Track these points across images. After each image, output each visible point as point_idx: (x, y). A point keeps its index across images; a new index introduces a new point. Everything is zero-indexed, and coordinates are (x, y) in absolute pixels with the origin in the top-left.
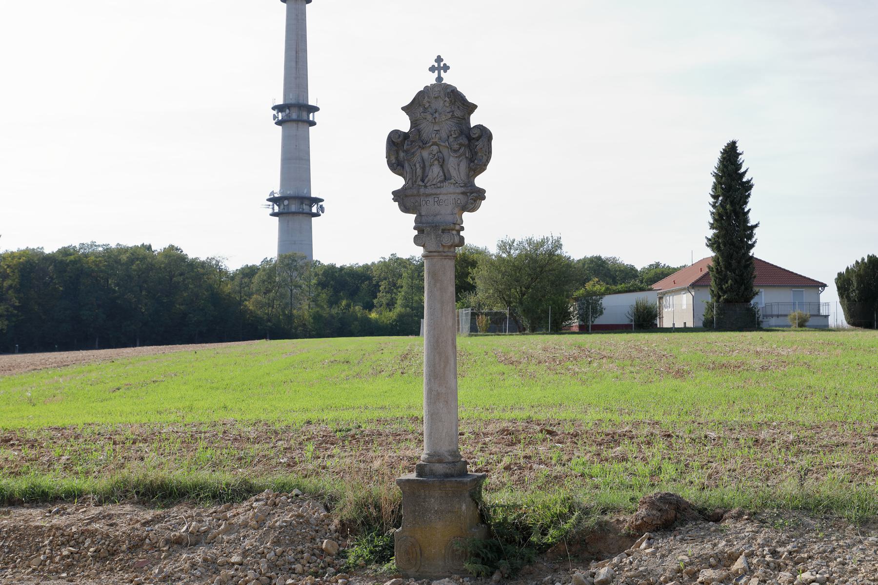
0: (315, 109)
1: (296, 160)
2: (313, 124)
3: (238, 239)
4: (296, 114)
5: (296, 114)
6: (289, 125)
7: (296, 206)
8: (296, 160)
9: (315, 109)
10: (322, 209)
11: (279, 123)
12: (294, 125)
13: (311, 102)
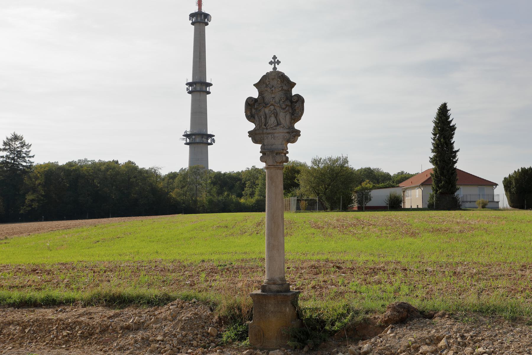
0: (210, 85)
1: (199, 113)
2: (209, 93)
3: (166, 157)
6: (196, 93)
8: (199, 113)
9: (210, 85)
10: (214, 141)
11: (190, 92)
12: (198, 93)
13: (208, 81)
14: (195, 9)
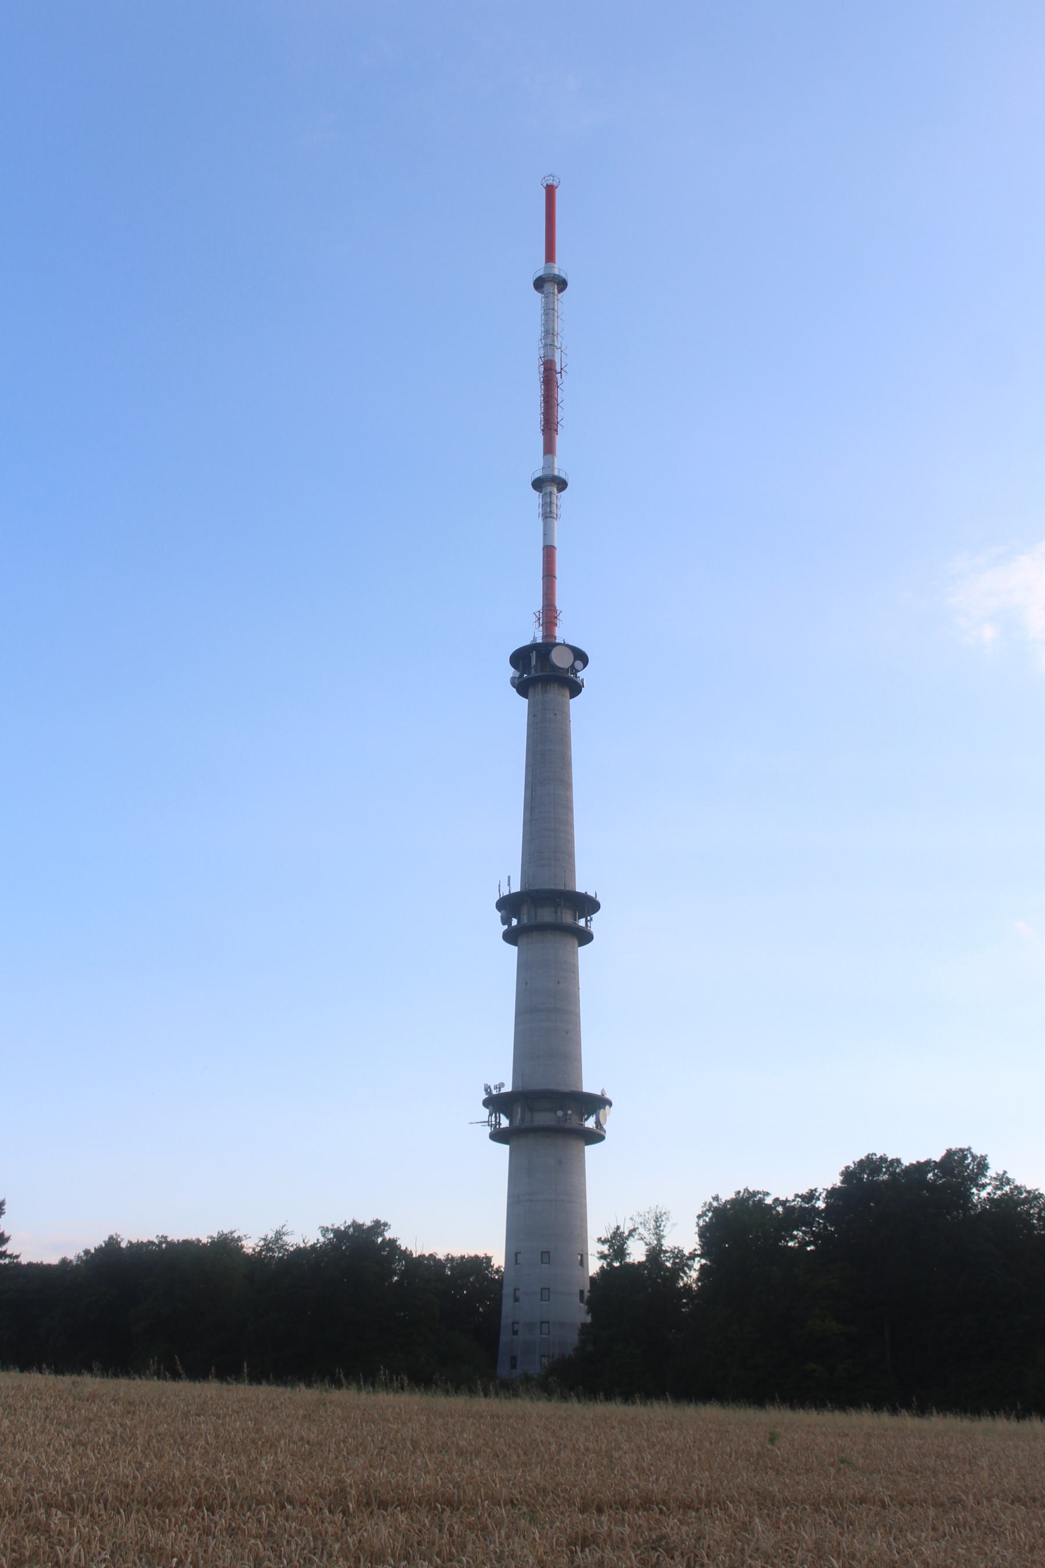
1: (546, 1015)
3: (453, 1208)
4: (547, 915)
5: (547, 915)
7: (545, 1117)
8: (546, 1015)
14: (531, 633)
